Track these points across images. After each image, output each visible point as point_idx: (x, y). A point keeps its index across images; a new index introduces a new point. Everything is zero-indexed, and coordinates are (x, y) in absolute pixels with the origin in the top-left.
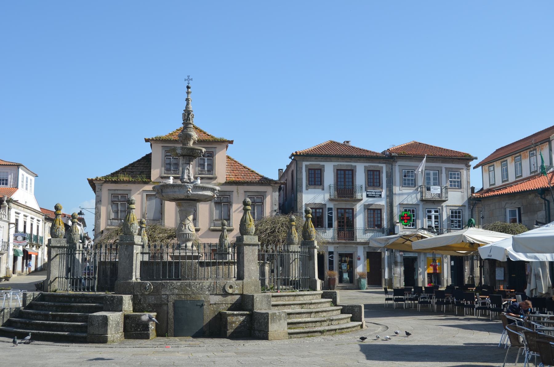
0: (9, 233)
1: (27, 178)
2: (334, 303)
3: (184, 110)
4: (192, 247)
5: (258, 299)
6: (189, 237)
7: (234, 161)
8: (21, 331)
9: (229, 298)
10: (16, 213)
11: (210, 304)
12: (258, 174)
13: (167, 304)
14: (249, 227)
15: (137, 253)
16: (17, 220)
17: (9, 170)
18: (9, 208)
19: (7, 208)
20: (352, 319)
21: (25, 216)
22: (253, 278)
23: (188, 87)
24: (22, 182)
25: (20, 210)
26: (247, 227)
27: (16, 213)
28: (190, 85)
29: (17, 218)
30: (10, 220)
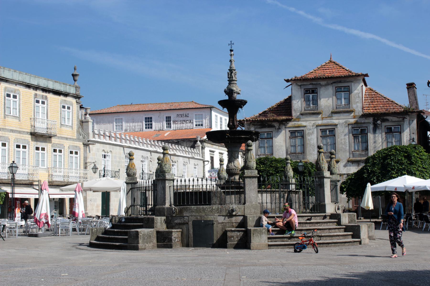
0: (204, 170)
1: (221, 118)
2: (339, 223)
3: (229, 70)
4: (239, 179)
5: (251, 219)
6: (236, 172)
7: (376, 92)
8: (101, 243)
9: (234, 219)
10: (210, 151)
11: (219, 223)
12: (397, 104)
13: (188, 223)
14: (250, 163)
15: (170, 187)
16: (212, 158)
17: (204, 112)
18: (202, 148)
19: (201, 148)
20: (353, 237)
21: (220, 153)
22: (254, 203)
23: (231, 51)
24: (216, 122)
25: (215, 148)
26: (248, 163)
27: (210, 151)
28: (232, 49)
29: (212, 156)
30: (204, 158)
